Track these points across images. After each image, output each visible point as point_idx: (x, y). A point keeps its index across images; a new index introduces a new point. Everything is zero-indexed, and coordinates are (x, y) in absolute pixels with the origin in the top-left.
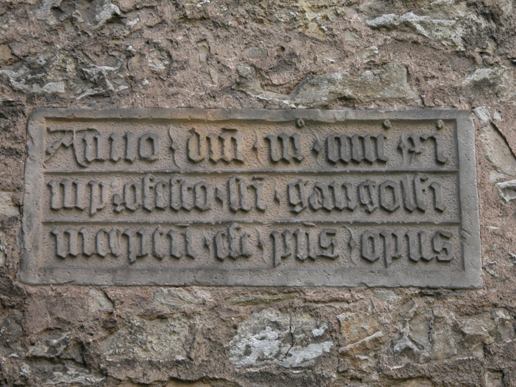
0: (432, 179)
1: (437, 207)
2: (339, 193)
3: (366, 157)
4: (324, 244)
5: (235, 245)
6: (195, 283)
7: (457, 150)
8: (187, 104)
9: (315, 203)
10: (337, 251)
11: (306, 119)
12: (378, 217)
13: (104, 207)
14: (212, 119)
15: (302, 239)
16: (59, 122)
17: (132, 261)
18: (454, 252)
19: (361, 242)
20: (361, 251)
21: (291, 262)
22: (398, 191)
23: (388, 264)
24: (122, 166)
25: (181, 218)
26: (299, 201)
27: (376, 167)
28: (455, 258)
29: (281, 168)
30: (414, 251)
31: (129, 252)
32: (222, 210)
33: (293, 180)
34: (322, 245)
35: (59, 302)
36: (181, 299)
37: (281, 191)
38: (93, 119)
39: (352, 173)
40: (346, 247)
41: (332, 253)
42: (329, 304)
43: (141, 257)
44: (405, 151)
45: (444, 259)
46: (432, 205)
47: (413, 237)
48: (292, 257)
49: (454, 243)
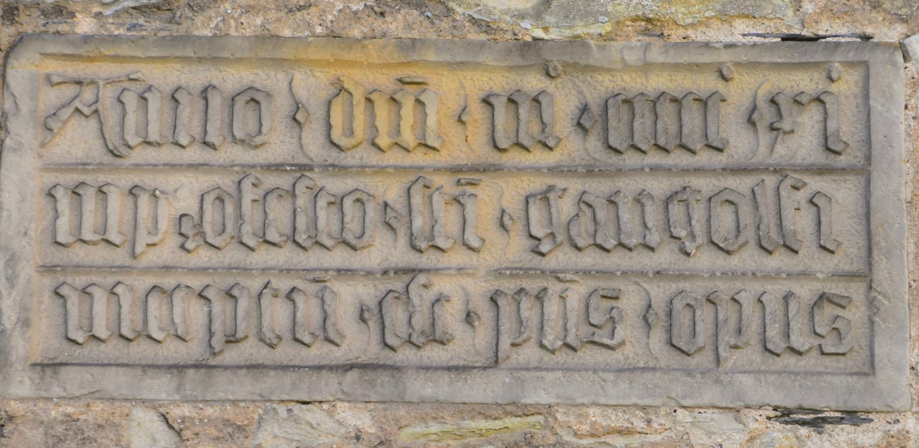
0: (815, 184)
1: (822, 243)
2: (628, 216)
3: (684, 141)
4: (595, 318)
5: (420, 321)
6: (340, 396)
7: (868, 127)
8: (327, 27)
9: (580, 236)
10: (621, 333)
11: (565, 62)
12: (705, 260)
13: (162, 241)
14: (377, 62)
15: (552, 307)
16: (68, 63)
17: (217, 350)
18: (855, 335)
19: (670, 314)
20: (669, 330)
21: (529, 353)
22: (745, 210)
23: (721, 359)
24: (195, 154)
25: (314, 259)
26: (550, 231)
27: (705, 158)
28: (856, 348)
29: (515, 158)
30: (773, 332)
31: (211, 334)
32: (395, 247)
33: (536, 184)
34: (592, 321)
35: (71, 433)
36: (312, 427)
37: (512, 204)
38: (139, 58)
39: (655, 169)
40: (640, 323)
41: (612, 338)
42: (603, 439)
43: (232, 340)
44: (762, 126)
45: (833, 350)
46: (814, 237)
47: (773, 305)
48: (533, 341)
49: (856, 314)
